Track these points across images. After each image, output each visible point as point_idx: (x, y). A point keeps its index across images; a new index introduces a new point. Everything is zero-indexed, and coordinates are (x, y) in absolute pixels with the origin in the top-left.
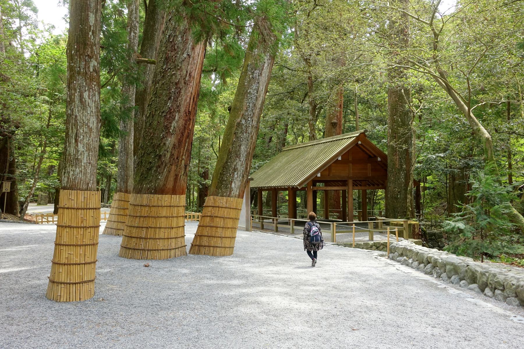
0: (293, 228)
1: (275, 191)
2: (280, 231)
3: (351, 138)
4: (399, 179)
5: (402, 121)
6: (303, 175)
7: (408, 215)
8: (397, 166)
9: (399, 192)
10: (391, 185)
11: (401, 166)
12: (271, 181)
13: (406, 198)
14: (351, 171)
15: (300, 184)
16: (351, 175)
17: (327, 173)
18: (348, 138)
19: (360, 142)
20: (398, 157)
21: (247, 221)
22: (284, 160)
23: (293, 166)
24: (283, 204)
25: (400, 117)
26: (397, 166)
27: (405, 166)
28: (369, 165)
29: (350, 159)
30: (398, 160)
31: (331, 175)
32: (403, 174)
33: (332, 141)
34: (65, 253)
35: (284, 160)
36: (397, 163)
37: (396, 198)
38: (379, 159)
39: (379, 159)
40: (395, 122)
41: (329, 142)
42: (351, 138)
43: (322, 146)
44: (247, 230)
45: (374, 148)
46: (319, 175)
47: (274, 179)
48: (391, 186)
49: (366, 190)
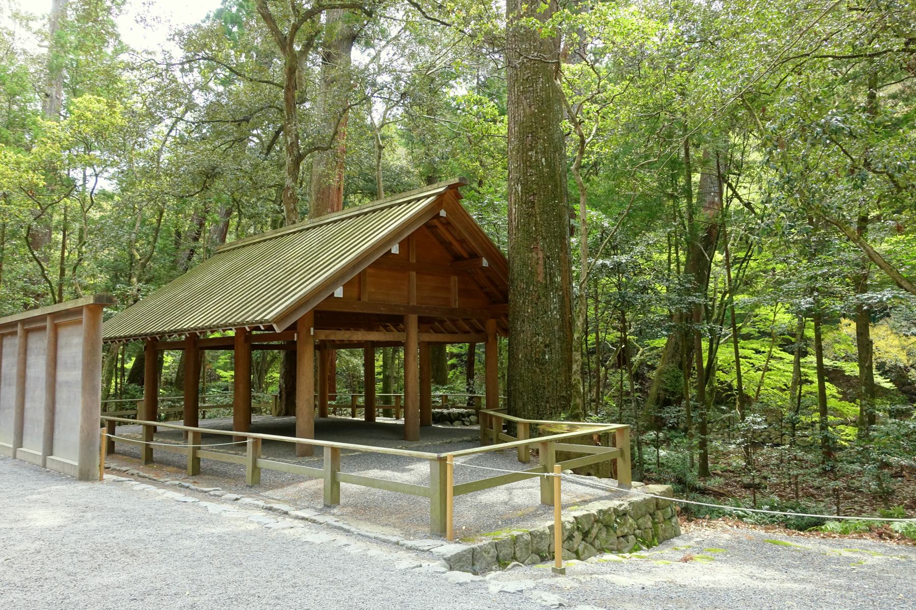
0: (255, 468)
1: (195, 345)
2: (205, 473)
3: (419, 199)
4: (546, 312)
5: (549, 165)
6: (284, 294)
7: (576, 407)
8: (540, 278)
9: (546, 346)
10: (526, 326)
11: (552, 276)
12: (183, 315)
13: (569, 362)
14: (414, 292)
15: (280, 319)
16: (414, 303)
17: (354, 293)
18: (409, 202)
19: (443, 213)
20: (541, 255)
21: (87, 443)
22: (222, 269)
23: (250, 275)
24: (213, 384)
25: (544, 153)
26: (540, 278)
27: (559, 279)
28: (454, 279)
29: (413, 260)
30: (541, 262)
31: (365, 299)
32: (554, 301)
33: (358, 216)
34: (222, 367)
35: (222, 269)
36: (540, 269)
37: (541, 363)
38: (485, 263)
39: (485, 263)
40: (531, 167)
41: (350, 218)
42: (419, 199)
43: (334, 228)
44: (85, 475)
45: (475, 231)
46: (339, 293)
47: (192, 309)
48: (525, 330)
49: (441, 345)
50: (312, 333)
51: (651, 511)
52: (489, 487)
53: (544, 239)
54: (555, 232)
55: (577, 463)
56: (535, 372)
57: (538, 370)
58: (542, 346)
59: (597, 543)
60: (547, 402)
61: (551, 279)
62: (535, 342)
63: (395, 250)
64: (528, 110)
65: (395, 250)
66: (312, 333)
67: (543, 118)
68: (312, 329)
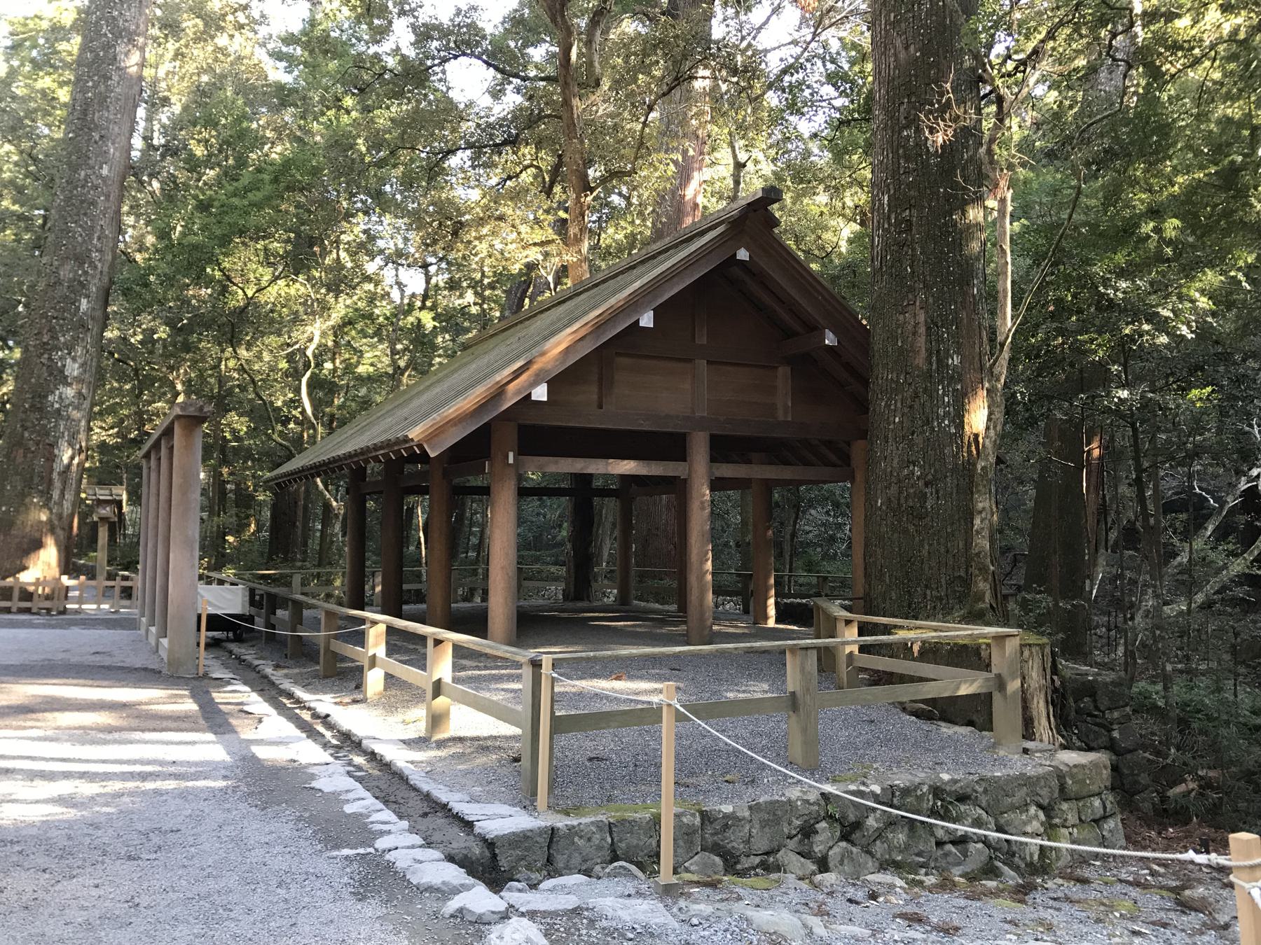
4: (928, 422)
10: (891, 446)
20: (922, 318)
30: (922, 330)
36: (921, 341)
38: (830, 340)
50: (511, 461)
51: (1045, 802)
52: (31, 676)
53: (927, 287)
54: (949, 273)
55: (906, 693)
56: (906, 531)
57: (912, 528)
58: (921, 483)
59: (879, 848)
60: (926, 587)
61: (939, 361)
62: (908, 477)
63: (647, 320)
64: (902, 55)
65: (647, 320)
66: (511, 461)
67: (931, 66)
68: (511, 455)
